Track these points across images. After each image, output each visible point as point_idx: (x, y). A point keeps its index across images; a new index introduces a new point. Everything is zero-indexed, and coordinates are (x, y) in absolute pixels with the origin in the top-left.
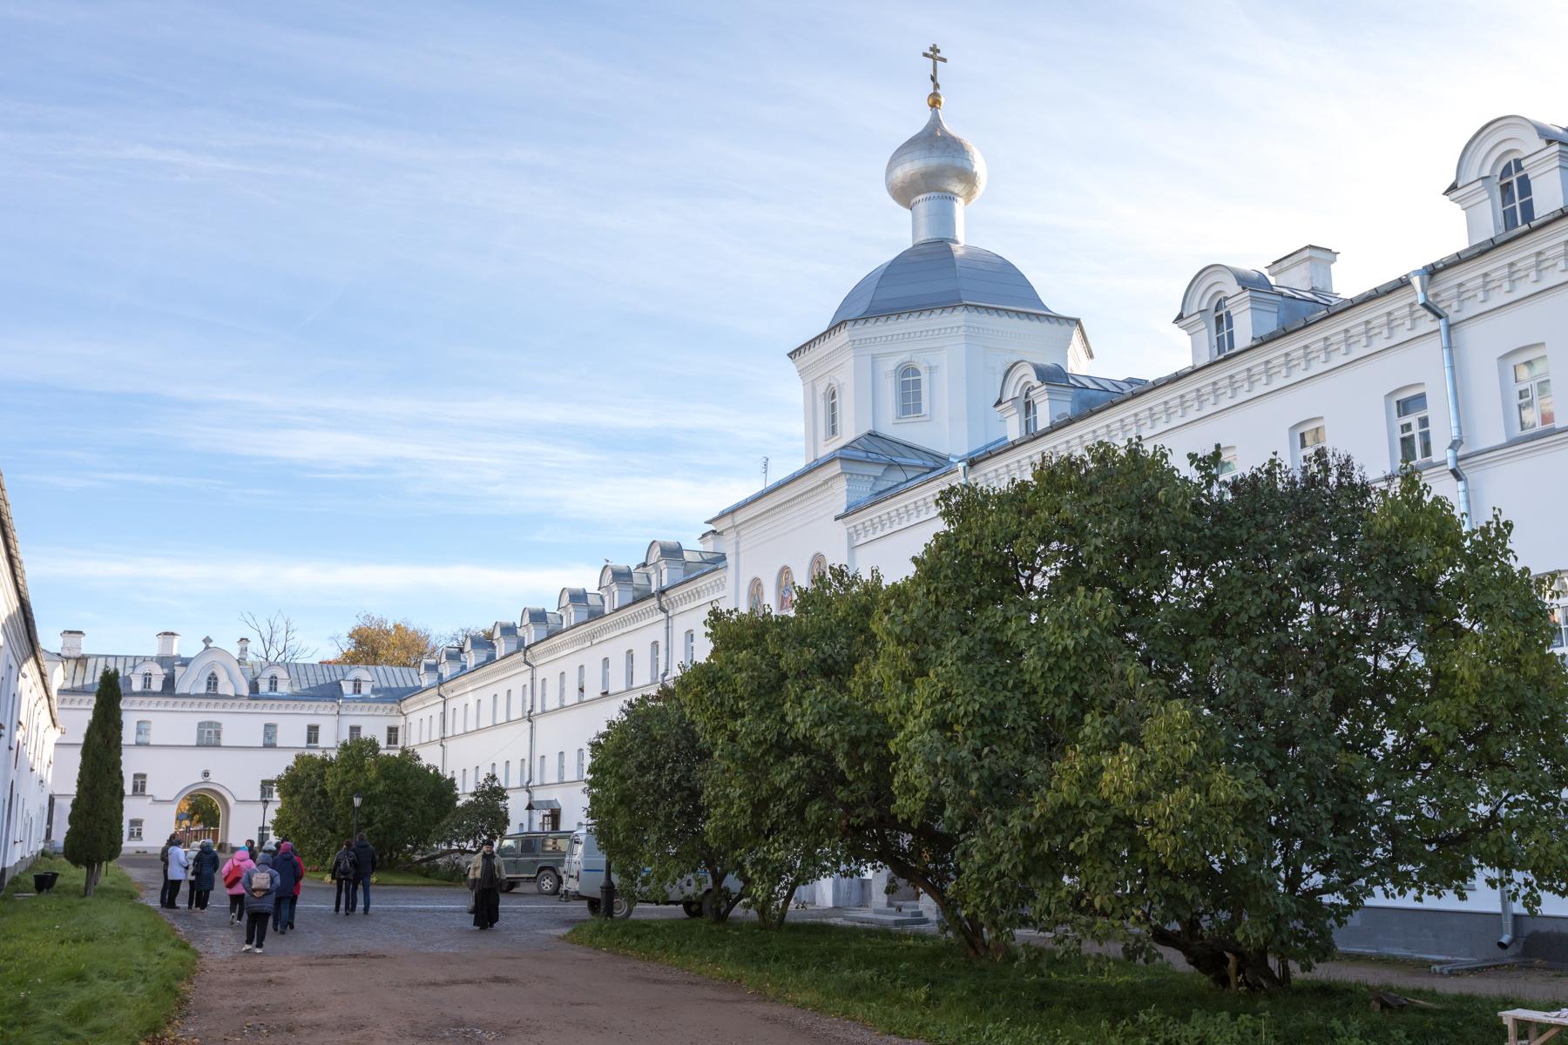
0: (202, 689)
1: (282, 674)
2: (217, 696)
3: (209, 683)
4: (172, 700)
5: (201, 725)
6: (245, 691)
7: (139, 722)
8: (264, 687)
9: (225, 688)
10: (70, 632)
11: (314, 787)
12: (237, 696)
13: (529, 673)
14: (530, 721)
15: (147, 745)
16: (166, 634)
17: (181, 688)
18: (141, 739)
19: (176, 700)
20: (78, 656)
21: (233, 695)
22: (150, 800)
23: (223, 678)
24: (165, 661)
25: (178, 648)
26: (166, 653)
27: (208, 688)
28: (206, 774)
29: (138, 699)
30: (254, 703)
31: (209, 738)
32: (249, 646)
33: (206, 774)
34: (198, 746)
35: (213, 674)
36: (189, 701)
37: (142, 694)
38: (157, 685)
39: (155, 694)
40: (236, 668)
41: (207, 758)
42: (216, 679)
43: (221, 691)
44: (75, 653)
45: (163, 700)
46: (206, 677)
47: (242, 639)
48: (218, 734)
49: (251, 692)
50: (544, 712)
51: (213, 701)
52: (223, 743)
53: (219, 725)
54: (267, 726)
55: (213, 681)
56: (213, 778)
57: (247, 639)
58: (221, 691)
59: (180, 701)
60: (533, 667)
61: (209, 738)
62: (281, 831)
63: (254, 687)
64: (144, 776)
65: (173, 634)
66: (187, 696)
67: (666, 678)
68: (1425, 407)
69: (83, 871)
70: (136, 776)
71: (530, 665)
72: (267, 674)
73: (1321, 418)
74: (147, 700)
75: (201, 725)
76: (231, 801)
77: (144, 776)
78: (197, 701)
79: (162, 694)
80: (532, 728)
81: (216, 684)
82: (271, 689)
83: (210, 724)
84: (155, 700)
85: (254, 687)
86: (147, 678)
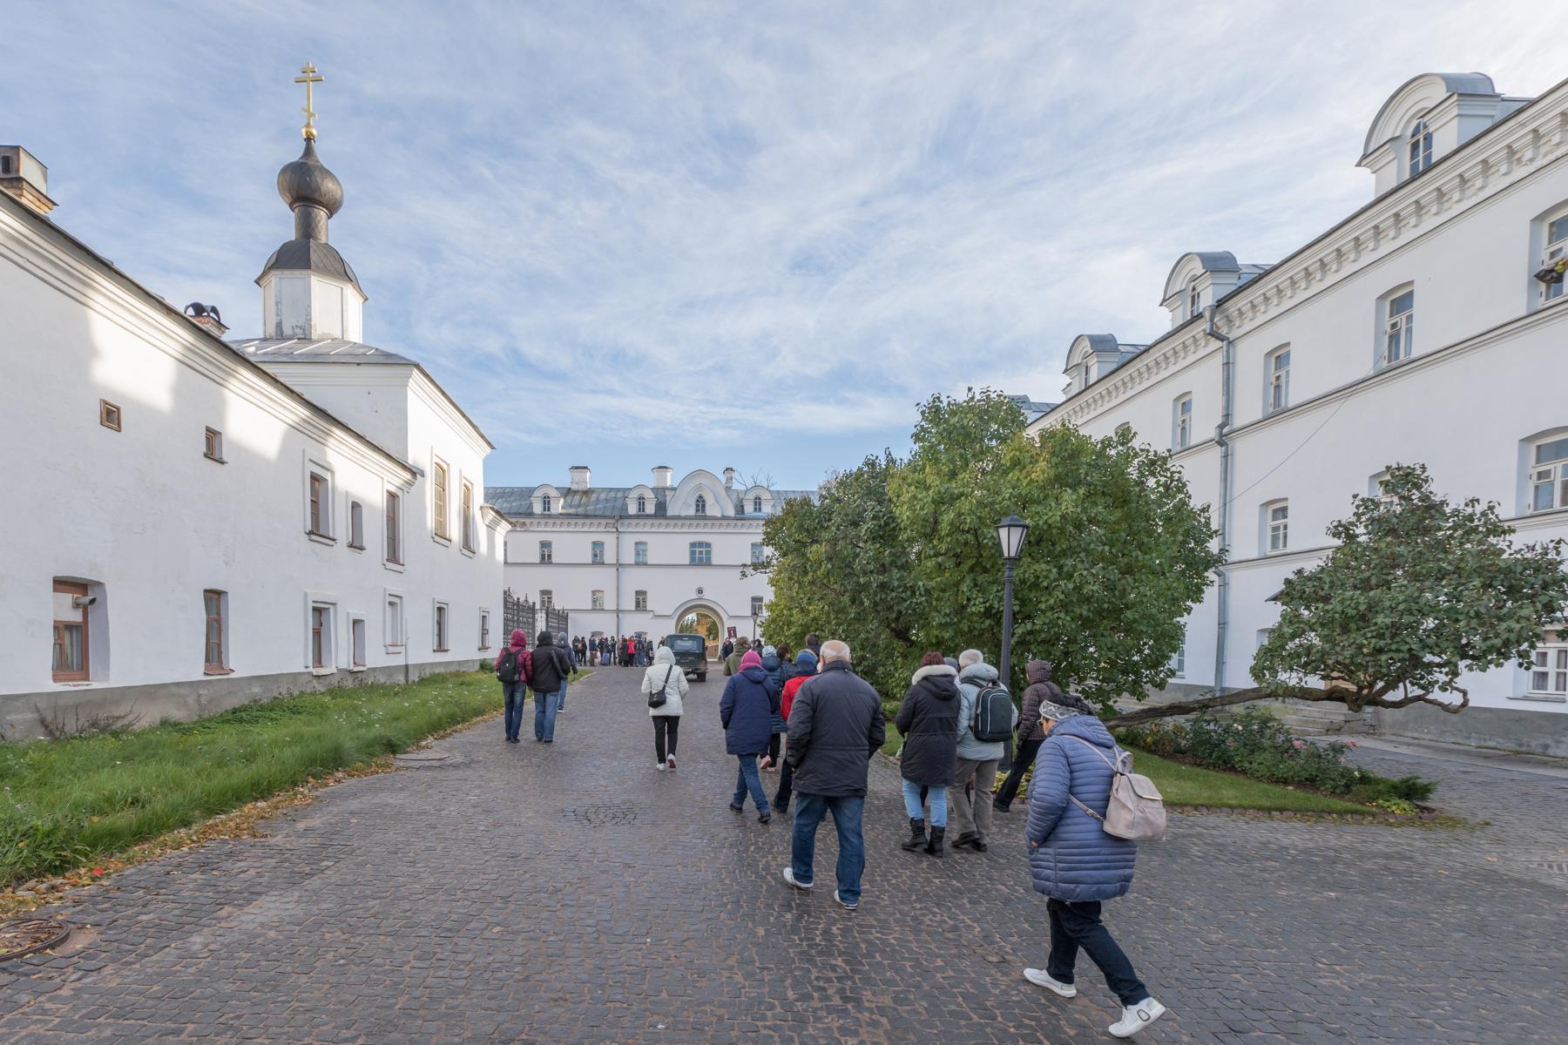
0: (692, 512)
1: (765, 496)
2: (705, 518)
3: (697, 506)
4: (664, 522)
5: (693, 545)
6: (731, 512)
7: (636, 543)
8: (749, 508)
9: (712, 510)
10: (577, 468)
11: (855, 524)
12: (724, 518)
13: (1215, 366)
14: (1221, 443)
15: (646, 564)
16: (660, 467)
17: (671, 511)
18: (641, 559)
19: (668, 521)
20: (585, 489)
21: (720, 516)
22: (651, 615)
23: (709, 501)
24: (660, 492)
25: (670, 480)
26: (661, 485)
27: (697, 511)
28: (700, 591)
29: (634, 522)
30: (740, 523)
31: (700, 557)
32: (735, 475)
33: (700, 591)
34: (690, 565)
35: (701, 497)
36: (680, 522)
37: (637, 517)
38: (650, 509)
39: (648, 516)
40: (723, 493)
41: (701, 576)
42: (704, 501)
43: (709, 512)
44: (581, 487)
45: (657, 522)
46: (694, 500)
47: (727, 469)
48: (708, 553)
49: (737, 512)
50: (1277, 411)
51: (702, 522)
52: (714, 562)
53: (708, 545)
54: (595, 544)
55: (701, 503)
56: (706, 595)
57: (731, 469)
58: (709, 512)
59: (672, 522)
60: (1230, 343)
61: (700, 557)
62: (776, 638)
63: (740, 508)
64: (644, 593)
65: (666, 468)
66: (679, 518)
67: (1225, 430)
68: (1285, 517)
69: (1002, 745)
70: (638, 593)
71: (1221, 338)
72: (751, 496)
73: (1286, 499)
74: (642, 522)
75: (693, 545)
76: (724, 617)
77: (644, 593)
78: (688, 522)
79: (655, 516)
80: (1226, 456)
81: (704, 506)
82: (755, 509)
83: (701, 544)
84: (649, 522)
85: (740, 508)
86: (641, 501)
